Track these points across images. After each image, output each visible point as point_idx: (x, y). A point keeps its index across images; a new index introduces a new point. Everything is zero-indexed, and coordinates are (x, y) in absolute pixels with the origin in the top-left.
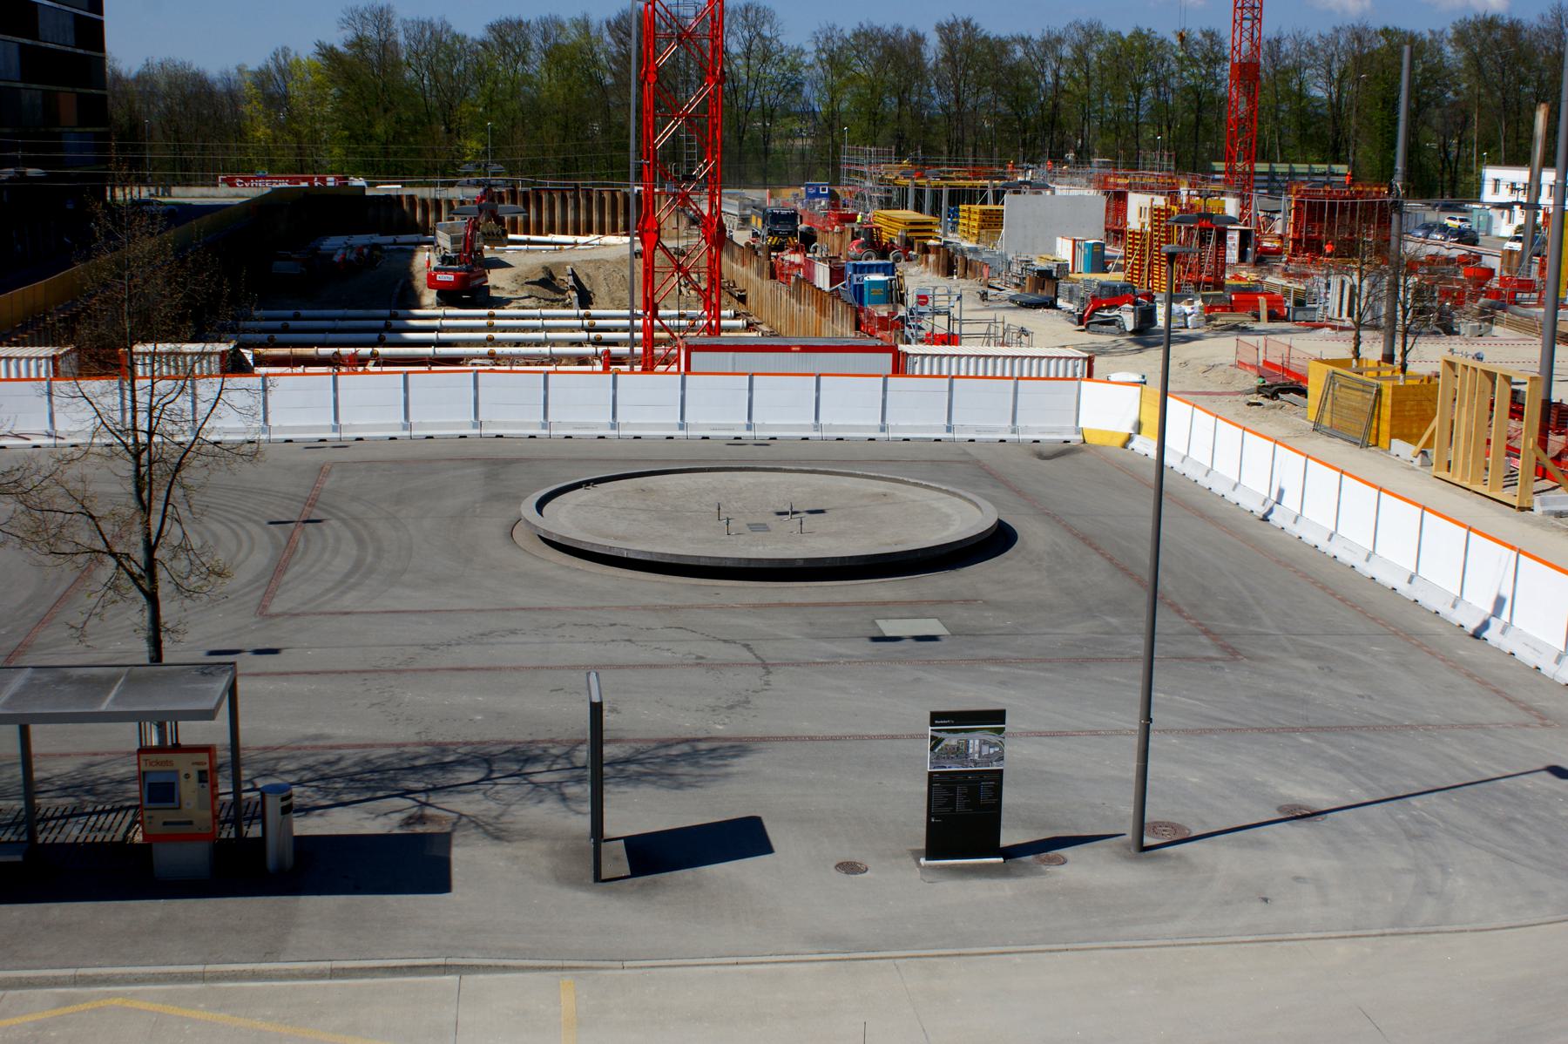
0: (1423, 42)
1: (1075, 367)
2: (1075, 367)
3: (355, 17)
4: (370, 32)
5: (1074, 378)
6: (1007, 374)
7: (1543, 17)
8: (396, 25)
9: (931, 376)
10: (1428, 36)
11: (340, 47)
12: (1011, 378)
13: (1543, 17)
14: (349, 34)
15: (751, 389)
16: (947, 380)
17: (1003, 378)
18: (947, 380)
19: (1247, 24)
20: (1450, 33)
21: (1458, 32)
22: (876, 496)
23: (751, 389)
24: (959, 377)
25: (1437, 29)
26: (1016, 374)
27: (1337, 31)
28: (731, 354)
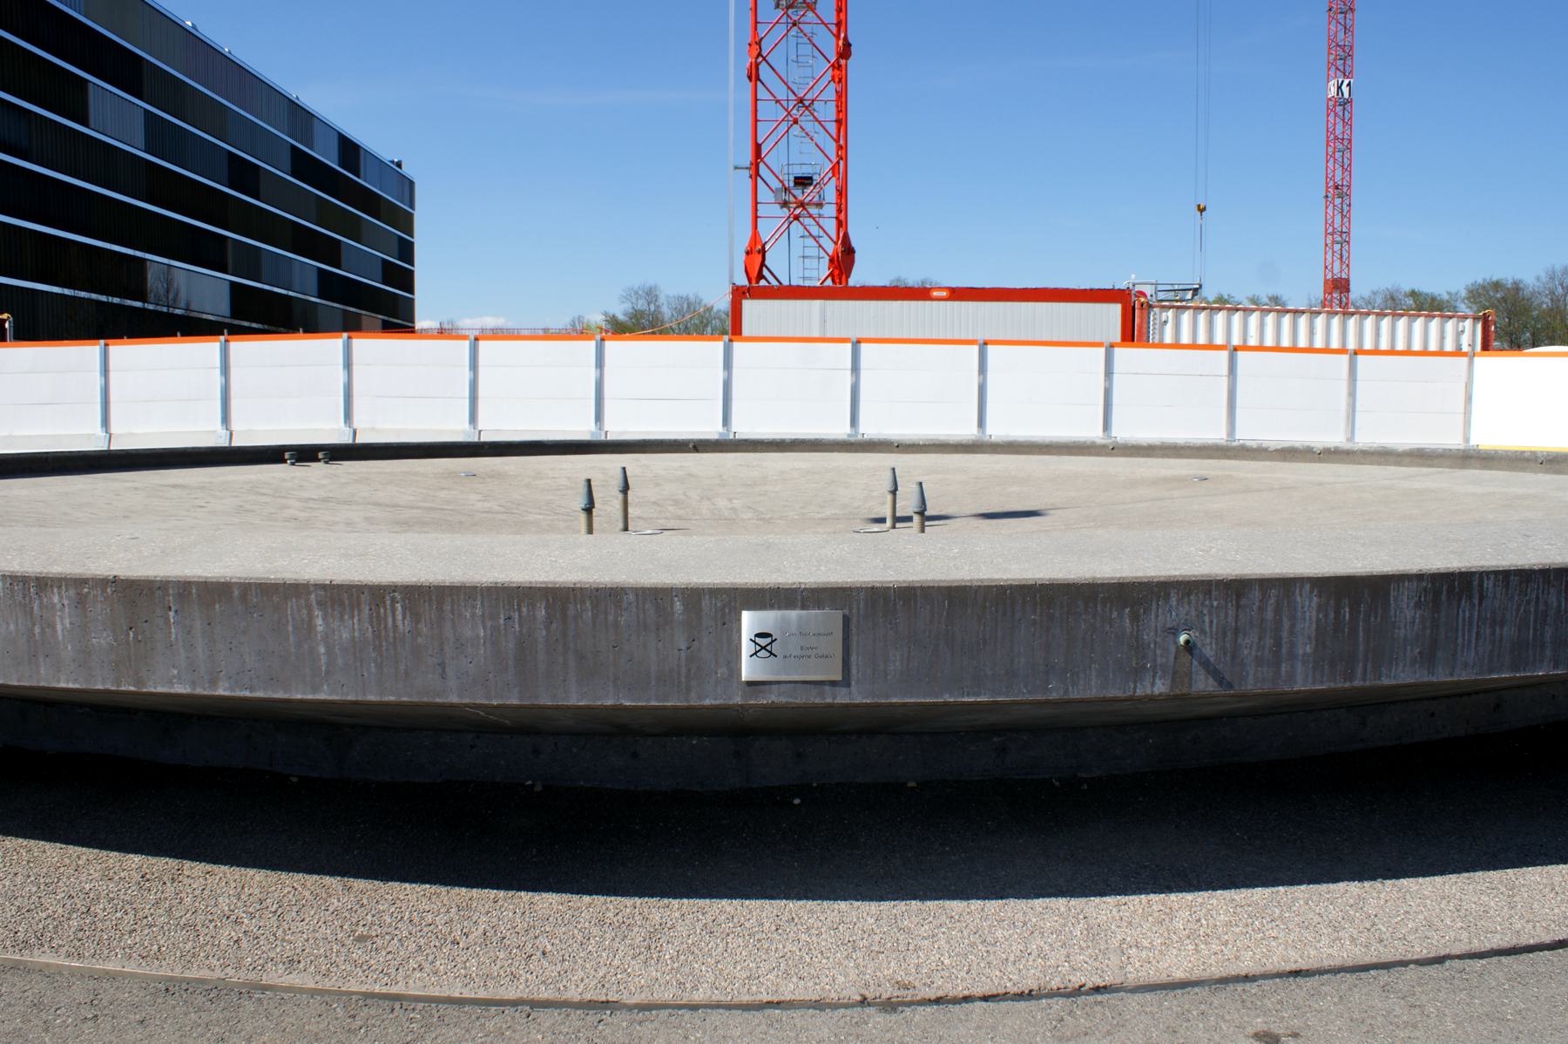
0: (1442, 301)
1: (1459, 334)
2: (1459, 334)
3: (633, 294)
4: (641, 305)
5: (1458, 352)
6: (1335, 344)
7: (1538, 279)
8: (662, 300)
9: (1194, 346)
10: (1446, 297)
11: (621, 317)
12: (1342, 351)
13: (1538, 279)
14: (627, 306)
15: (855, 368)
16: (1224, 354)
17: (1327, 350)
18: (1224, 354)
19: (1337, 247)
20: (1463, 293)
21: (1471, 292)
22: (1182, 481)
23: (855, 368)
24: (1245, 347)
25: (1453, 291)
26: (1351, 345)
27: (1375, 293)
28: (817, 304)
